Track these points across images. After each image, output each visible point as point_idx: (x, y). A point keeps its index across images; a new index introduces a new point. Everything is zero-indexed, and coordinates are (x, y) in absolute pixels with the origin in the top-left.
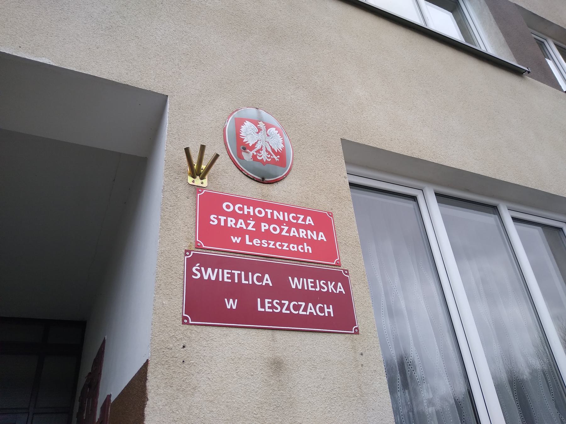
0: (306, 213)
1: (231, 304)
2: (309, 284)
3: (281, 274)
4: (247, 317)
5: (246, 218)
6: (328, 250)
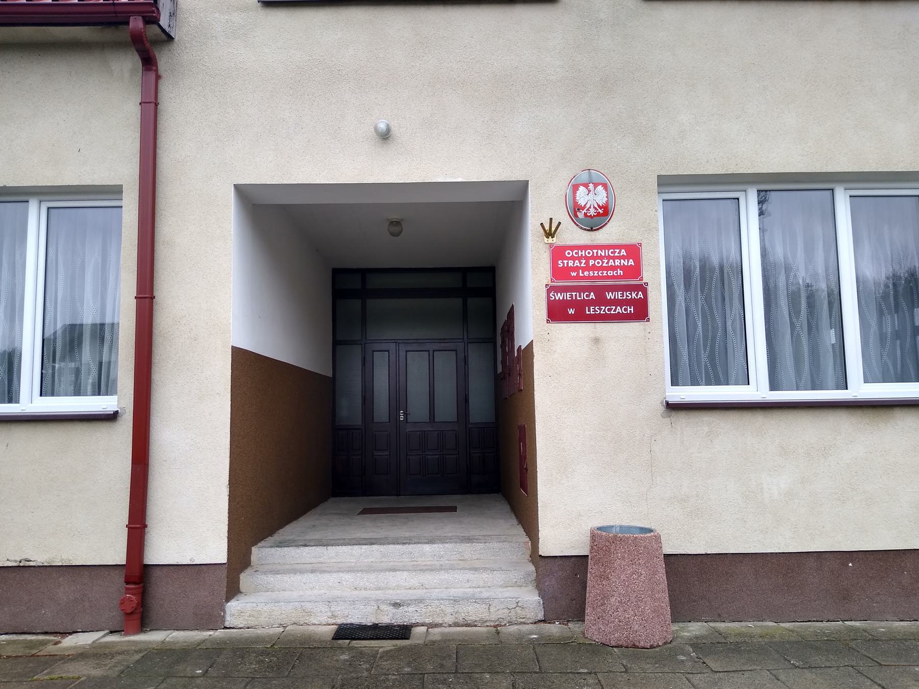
0: (620, 247)
1: (571, 311)
2: (619, 295)
3: (600, 291)
4: (581, 317)
5: (579, 259)
6: (635, 271)
